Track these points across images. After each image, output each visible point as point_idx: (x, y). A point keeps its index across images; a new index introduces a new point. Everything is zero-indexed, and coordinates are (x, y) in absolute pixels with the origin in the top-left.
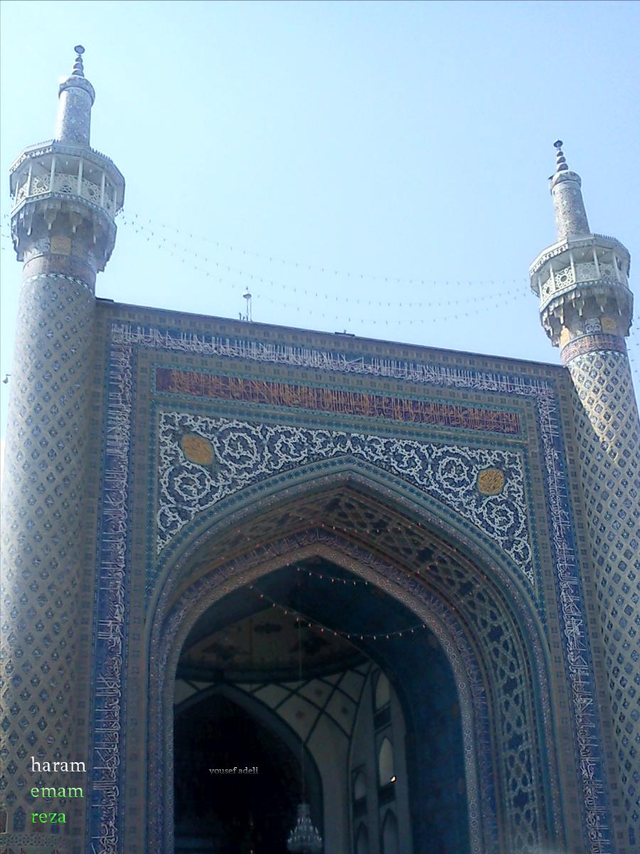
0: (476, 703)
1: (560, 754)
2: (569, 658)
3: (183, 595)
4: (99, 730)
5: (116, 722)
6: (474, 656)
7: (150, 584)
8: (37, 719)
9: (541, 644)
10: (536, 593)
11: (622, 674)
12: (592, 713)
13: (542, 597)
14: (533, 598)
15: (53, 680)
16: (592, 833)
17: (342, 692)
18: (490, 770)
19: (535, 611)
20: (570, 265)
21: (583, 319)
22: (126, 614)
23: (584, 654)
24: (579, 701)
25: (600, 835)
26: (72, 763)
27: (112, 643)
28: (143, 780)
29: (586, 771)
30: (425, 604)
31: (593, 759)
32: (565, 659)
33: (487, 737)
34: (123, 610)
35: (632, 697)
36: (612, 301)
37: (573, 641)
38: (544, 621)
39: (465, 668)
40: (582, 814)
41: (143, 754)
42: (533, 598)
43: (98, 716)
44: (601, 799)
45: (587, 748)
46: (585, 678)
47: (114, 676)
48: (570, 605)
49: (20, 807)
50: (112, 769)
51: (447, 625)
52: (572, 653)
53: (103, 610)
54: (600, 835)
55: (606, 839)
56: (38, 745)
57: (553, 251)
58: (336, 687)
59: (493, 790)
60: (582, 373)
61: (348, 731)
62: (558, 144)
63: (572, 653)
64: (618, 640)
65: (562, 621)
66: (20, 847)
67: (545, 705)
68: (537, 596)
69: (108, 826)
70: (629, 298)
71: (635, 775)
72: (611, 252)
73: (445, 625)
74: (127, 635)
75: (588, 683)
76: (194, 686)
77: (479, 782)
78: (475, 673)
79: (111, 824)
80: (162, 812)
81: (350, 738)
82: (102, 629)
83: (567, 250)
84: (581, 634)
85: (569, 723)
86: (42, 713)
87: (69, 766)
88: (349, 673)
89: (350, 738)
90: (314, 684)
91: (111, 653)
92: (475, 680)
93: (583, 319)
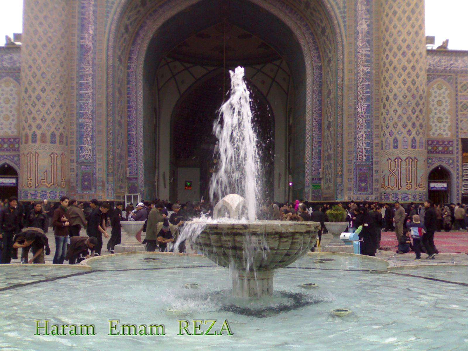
0: (315, 72)
1: (345, 102)
2: (358, 44)
3: (147, 18)
4: (82, 92)
5: (90, 87)
6: (317, 45)
7: (108, 12)
8: (40, 88)
9: (341, 36)
10: (341, 5)
12: (369, 76)
13: (344, 7)
14: (339, 8)
15: (49, 67)
16: (360, 144)
19: (339, 16)
22: (95, 30)
23: (368, 42)
24: (361, 69)
25: (364, 145)
27: (87, 46)
28: (105, 117)
29: (360, 109)
30: (289, 16)
31: (366, 103)
32: (356, 44)
34: (93, 28)
37: (362, 33)
38: (344, 22)
39: (311, 52)
41: (104, 103)
42: (339, 8)
43: (81, 84)
44: (368, 125)
45: (363, 96)
46: (367, 55)
47: (89, 63)
48: (363, 12)
49: (34, 132)
50: (89, 112)
51: (302, 27)
52: (360, 41)
53: (83, 27)
54: (364, 145)
55: (368, 147)
56: (42, 100)
58: (279, 67)
63: (360, 41)
65: (356, 22)
66: (35, 151)
67: (340, 71)
68: (342, 7)
69: (88, 140)
73: (300, 28)
74: (96, 41)
75: (369, 58)
76: (255, 68)
78: (317, 55)
79: (89, 139)
80: (136, 133)
81: (287, 94)
82: (82, 38)
84: (368, 29)
85: (353, 82)
86: (43, 84)
89: (287, 94)
91: (87, 51)
92: (316, 59)
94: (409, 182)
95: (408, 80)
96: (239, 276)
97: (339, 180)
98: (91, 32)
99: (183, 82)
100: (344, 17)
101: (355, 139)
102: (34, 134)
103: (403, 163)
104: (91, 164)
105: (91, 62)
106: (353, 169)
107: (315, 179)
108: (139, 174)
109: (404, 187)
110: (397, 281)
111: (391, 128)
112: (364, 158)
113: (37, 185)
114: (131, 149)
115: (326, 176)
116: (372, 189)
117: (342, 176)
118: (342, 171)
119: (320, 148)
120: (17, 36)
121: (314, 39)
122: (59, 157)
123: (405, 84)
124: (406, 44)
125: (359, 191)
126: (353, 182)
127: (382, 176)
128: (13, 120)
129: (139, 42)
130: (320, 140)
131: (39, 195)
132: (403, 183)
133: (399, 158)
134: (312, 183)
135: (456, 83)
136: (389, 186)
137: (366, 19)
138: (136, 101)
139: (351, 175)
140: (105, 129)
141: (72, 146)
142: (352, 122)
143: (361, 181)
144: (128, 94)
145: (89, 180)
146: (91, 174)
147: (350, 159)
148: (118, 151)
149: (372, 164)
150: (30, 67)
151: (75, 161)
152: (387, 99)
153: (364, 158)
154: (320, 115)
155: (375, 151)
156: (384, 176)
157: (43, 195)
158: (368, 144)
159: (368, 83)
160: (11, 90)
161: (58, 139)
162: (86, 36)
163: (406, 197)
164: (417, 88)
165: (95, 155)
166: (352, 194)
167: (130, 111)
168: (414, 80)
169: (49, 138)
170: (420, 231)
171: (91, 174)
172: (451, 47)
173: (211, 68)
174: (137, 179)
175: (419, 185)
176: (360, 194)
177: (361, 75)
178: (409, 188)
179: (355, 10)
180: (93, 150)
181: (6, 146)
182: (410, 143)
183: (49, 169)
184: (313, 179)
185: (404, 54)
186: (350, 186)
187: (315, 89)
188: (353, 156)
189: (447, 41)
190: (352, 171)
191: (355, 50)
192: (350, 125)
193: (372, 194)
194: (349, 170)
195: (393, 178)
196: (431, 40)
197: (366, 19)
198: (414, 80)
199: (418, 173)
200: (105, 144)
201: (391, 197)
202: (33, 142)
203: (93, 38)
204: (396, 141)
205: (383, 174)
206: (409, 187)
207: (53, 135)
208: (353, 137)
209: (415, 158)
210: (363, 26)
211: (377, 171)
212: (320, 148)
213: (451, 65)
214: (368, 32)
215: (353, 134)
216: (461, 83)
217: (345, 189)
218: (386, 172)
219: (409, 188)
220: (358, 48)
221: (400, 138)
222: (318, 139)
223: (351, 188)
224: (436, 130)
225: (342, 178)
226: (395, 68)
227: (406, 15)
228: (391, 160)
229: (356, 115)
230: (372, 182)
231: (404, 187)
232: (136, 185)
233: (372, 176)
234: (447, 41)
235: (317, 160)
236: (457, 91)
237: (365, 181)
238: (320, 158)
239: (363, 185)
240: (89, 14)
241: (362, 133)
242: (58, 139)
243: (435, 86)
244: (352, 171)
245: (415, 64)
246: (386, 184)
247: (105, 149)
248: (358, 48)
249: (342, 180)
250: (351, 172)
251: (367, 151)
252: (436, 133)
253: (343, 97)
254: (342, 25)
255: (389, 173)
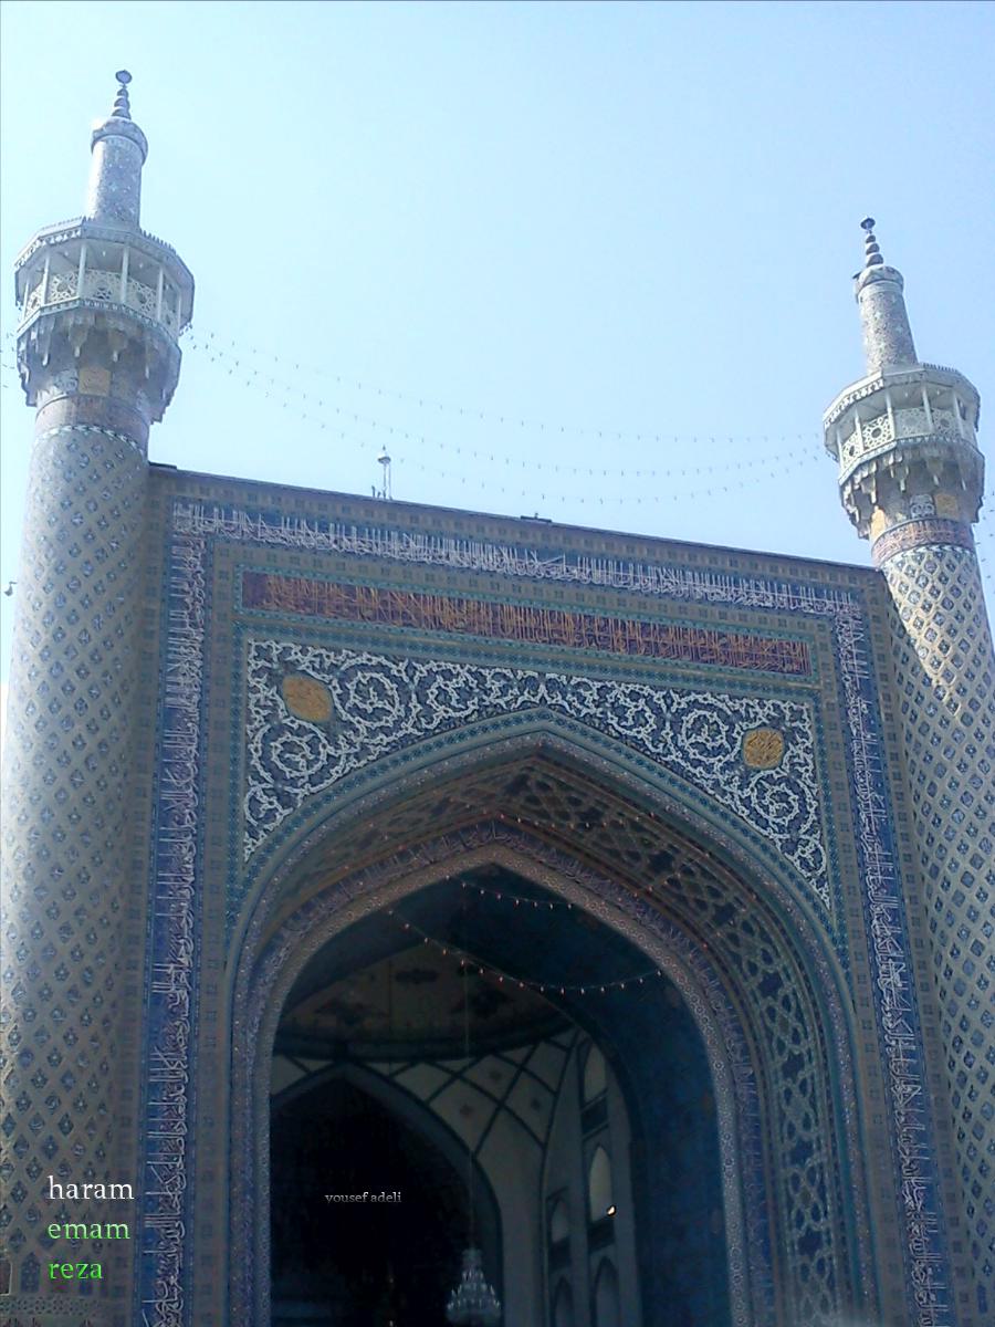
0: (740, 1092)
1: (870, 1172)
2: (884, 1022)
3: (284, 924)
4: (154, 1135)
5: (181, 1121)
6: (737, 1020)
7: (234, 907)
8: (58, 1118)
9: (841, 1001)
10: (834, 922)
11: (968, 1047)
12: (920, 1108)
13: (842, 927)
14: (829, 929)
15: (83, 1056)
16: (921, 1295)
17: (532, 1075)
18: (762, 1197)
19: (832, 949)
20: (886, 411)
21: (906, 495)
22: (196, 955)
23: (907, 1017)
24: (899, 1089)
25: (933, 1297)
26: (112, 1186)
27: (174, 999)
28: (222, 1211)
29: (910, 1198)
30: (661, 939)
31: (923, 1180)
32: (879, 1024)
33: (757, 1145)
34: (191, 948)
35: (983, 1082)
36: (952, 468)
37: (891, 996)
38: (845, 965)
39: (723, 1038)
40: (905, 1264)
41: (222, 1172)
42: (829, 929)
43: (152, 1112)
44: (935, 1242)
45: (912, 1162)
46: (909, 1054)
47: (178, 1050)
48: (887, 940)
49: (32, 1254)
50: (175, 1195)
51: (696, 971)
52: (889, 1015)
53: (161, 948)
54: (933, 1297)
55: (942, 1303)
56: (59, 1157)
57: (859, 391)
58: (522, 1068)
59: (766, 1227)
60: (906, 579)
61: (542, 1137)
62: (868, 224)
63: (889, 1015)
64: (961, 995)
65: (874, 966)
67: (847, 1096)
68: (835, 927)
69: (168, 1284)
70: (978, 463)
71: (987, 1205)
72: (950, 392)
73: (691, 971)
74: (198, 986)
75: (914, 1061)
76: (301, 1067)
77: (744, 1215)
78: (739, 1045)
79: (173, 1280)
80: (252, 1261)
81: (544, 1146)
82: (158, 977)
83: (882, 388)
84: (904, 986)
85: (885, 1124)
86: (66, 1108)
87: (108, 1190)
88: (542, 1046)
89: (544, 1146)
90: (489, 1063)
91: (173, 1015)
92: (738, 1057)
93: (906, 495)
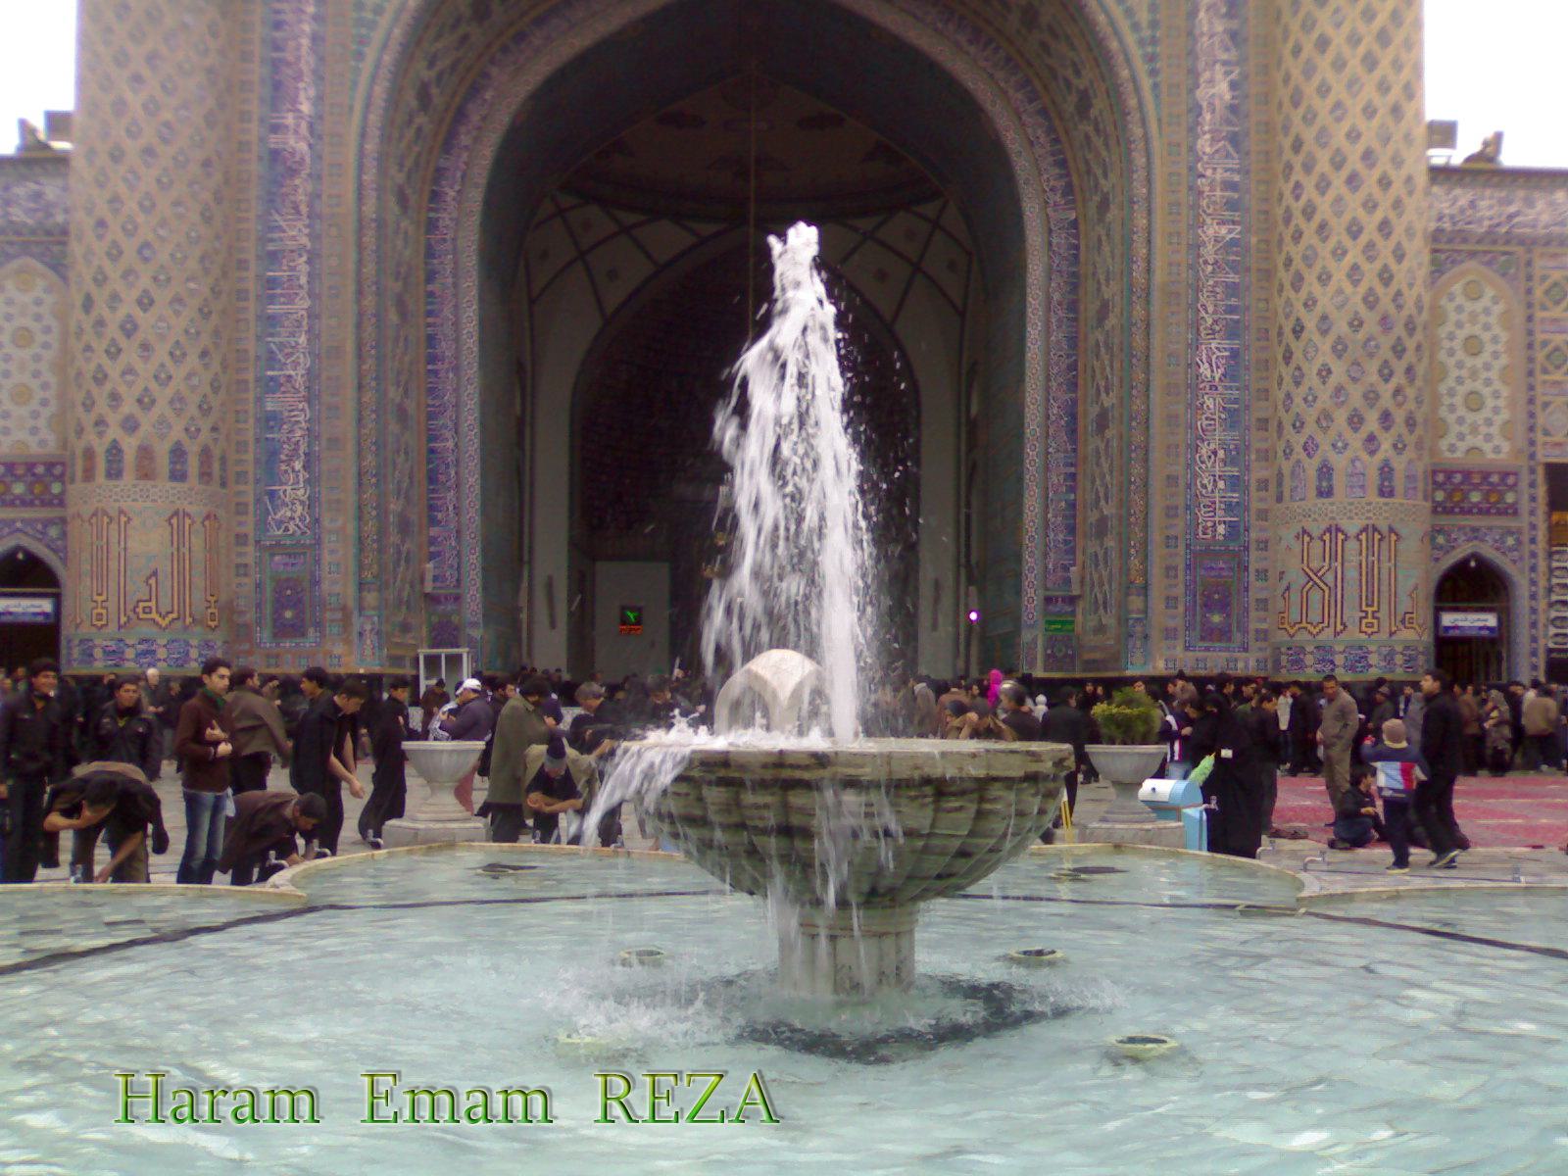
0: (1055, 241)
1: (1157, 340)
2: (1199, 146)
3: (492, 61)
4: (274, 309)
5: (303, 293)
6: (1061, 152)
7: (363, 41)
8: (135, 294)
9: (1144, 122)
10: (1144, 16)
12: (1237, 254)
13: (1154, 24)
14: (1136, 27)
15: (163, 223)
16: (1205, 481)
19: (1137, 53)
22: (319, 99)
23: (1234, 140)
24: (1211, 232)
25: (1221, 484)
27: (293, 154)
28: (351, 392)
29: (1207, 365)
30: (967, 53)
31: (1226, 344)
32: (1192, 149)
34: (312, 93)
37: (1213, 112)
38: (1153, 73)
39: (1040, 175)
41: (350, 346)
42: (1136, 27)
43: (272, 283)
44: (1233, 417)
45: (1215, 322)
46: (1229, 185)
47: (298, 212)
48: (1216, 39)
49: (115, 441)
50: (299, 375)
51: (1011, 92)
52: (1208, 136)
53: (278, 92)
54: (1221, 484)
55: (1234, 491)
56: (139, 336)
58: (936, 224)
63: (1208, 136)
65: (1194, 73)
66: (117, 505)
67: (1139, 239)
68: (1144, 24)
69: (293, 470)
73: (1005, 93)
74: (320, 137)
75: (1236, 196)
76: (856, 229)
78: (1062, 183)
79: (298, 465)
80: (456, 445)
81: (962, 314)
82: (276, 129)
84: (1233, 98)
85: (1184, 275)
86: (145, 282)
89: (962, 314)
91: (293, 172)
92: (1058, 198)
94: (1370, 610)
95: (1366, 266)
96: (801, 925)
97: (1136, 602)
98: (306, 108)
99: (613, 275)
100: (1151, 58)
101: (1188, 466)
102: (115, 450)
103: (1352, 545)
104: (306, 549)
105: (304, 209)
106: (1181, 567)
107: (1057, 598)
108: (466, 581)
109: (1353, 628)
110: (1331, 943)
111: (1310, 428)
112: (1221, 529)
113: (123, 619)
114: (439, 499)
115: (1092, 590)
116: (1246, 632)
117: (1145, 589)
118: (1145, 573)
119: (1072, 496)
120: (57, 122)
121: (1051, 130)
122: (198, 526)
123: (1356, 283)
124: (1360, 147)
125: (1202, 639)
126: (1181, 609)
127: (1280, 591)
128: (44, 403)
129: (465, 139)
130: (1072, 470)
131: (130, 653)
132: (1352, 614)
133: (1338, 530)
134: (1046, 612)
135: (1529, 278)
136: (1304, 624)
137: (1225, 63)
138: (457, 340)
139: (1176, 586)
140: (351, 432)
141: (242, 488)
142: (1180, 408)
143: (1208, 606)
144: (429, 314)
145: (297, 604)
146: (306, 584)
147: (1172, 532)
148: (395, 506)
149: (1247, 549)
150: (101, 223)
151: (251, 540)
152: (1298, 330)
153: (1221, 529)
154: (1073, 385)
155: (1255, 505)
156: (1288, 588)
157: (145, 653)
158: (1234, 483)
159: (1233, 278)
160: (38, 302)
161: (193, 465)
162: (290, 119)
163: (1360, 659)
164: (1399, 294)
165: (317, 521)
166: (1179, 649)
167: (436, 373)
168: (1386, 268)
169: (163, 463)
170: (1406, 773)
171: (306, 584)
172: (1510, 157)
173: (708, 229)
174: (457, 598)
175: (1403, 621)
176: (1207, 649)
177: (1209, 252)
178: (1369, 631)
179: (1190, 33)
180: (312, 503)
181: (19, 489)
182: (1373, 477)
183: (164, 567)
184: (1048, 600)
185: (1353, 181)
186: (1171, 624)
187: (1056, 297)
188: (1181, 524)
189: (1498, 138)
190: (1181, 574)
191: (1190, 169)
192: (1171, 419)
193: (1246, 650)
194: (1170, 570)
195: (1315, 596)
196: (1445, 133)
197: (1225, 63)
198: (1386, 268)
199: (1400, 578)
200: (351, 483)
201: (1309, 660)
202: (109, 475)
203: (311, 126)
204: (1325, 471)
205: (1284, 583)
206: (1371, 625)
207: (178, 453)
208: (1182, 460)
209: (1391, 530)
210: (1217, 88)
211: (1262, 574)
212: (1072, 496)
213: (1511, 217)
214: (1233, 109)
215: (1182, 449)
216: (1544, 278)
217: (1155, 635)
218: (1295, 576)
219: (1369, 631)
220: (1199, 159)
221: (1339, 462)
222: (1067, 465)
223: (1176, 629)
224: (1461, 437)
225: (1146, 595)
226: (1322, 227)
227: (1362, 50)
228: (1309, 535)
229: (1194, 385)
230: (1247, 610)
231: (1353, 628)
232: (455, 619)
233: (1247, 589)
234: (1498, 138)
235: (1061, 537)
236: (1530, 305)
237: (1224, 606)
238: (1072, 530)
239: (1216, 618)
240: (298, 47)
241: (1212, 446)
242: (193, 465)
243: (1457, 288)
244: (1181, 574)
245: (1392, 215)
246: (1295, 615)
247: (351, 499)
248: (1199, 159)
249: (1146, 601)
250: (1176, 576)
251: (1230, 508)
252: (1462, 446)
253: (1148, 326)
254: (1146, 83)
255: (1303, 580)
